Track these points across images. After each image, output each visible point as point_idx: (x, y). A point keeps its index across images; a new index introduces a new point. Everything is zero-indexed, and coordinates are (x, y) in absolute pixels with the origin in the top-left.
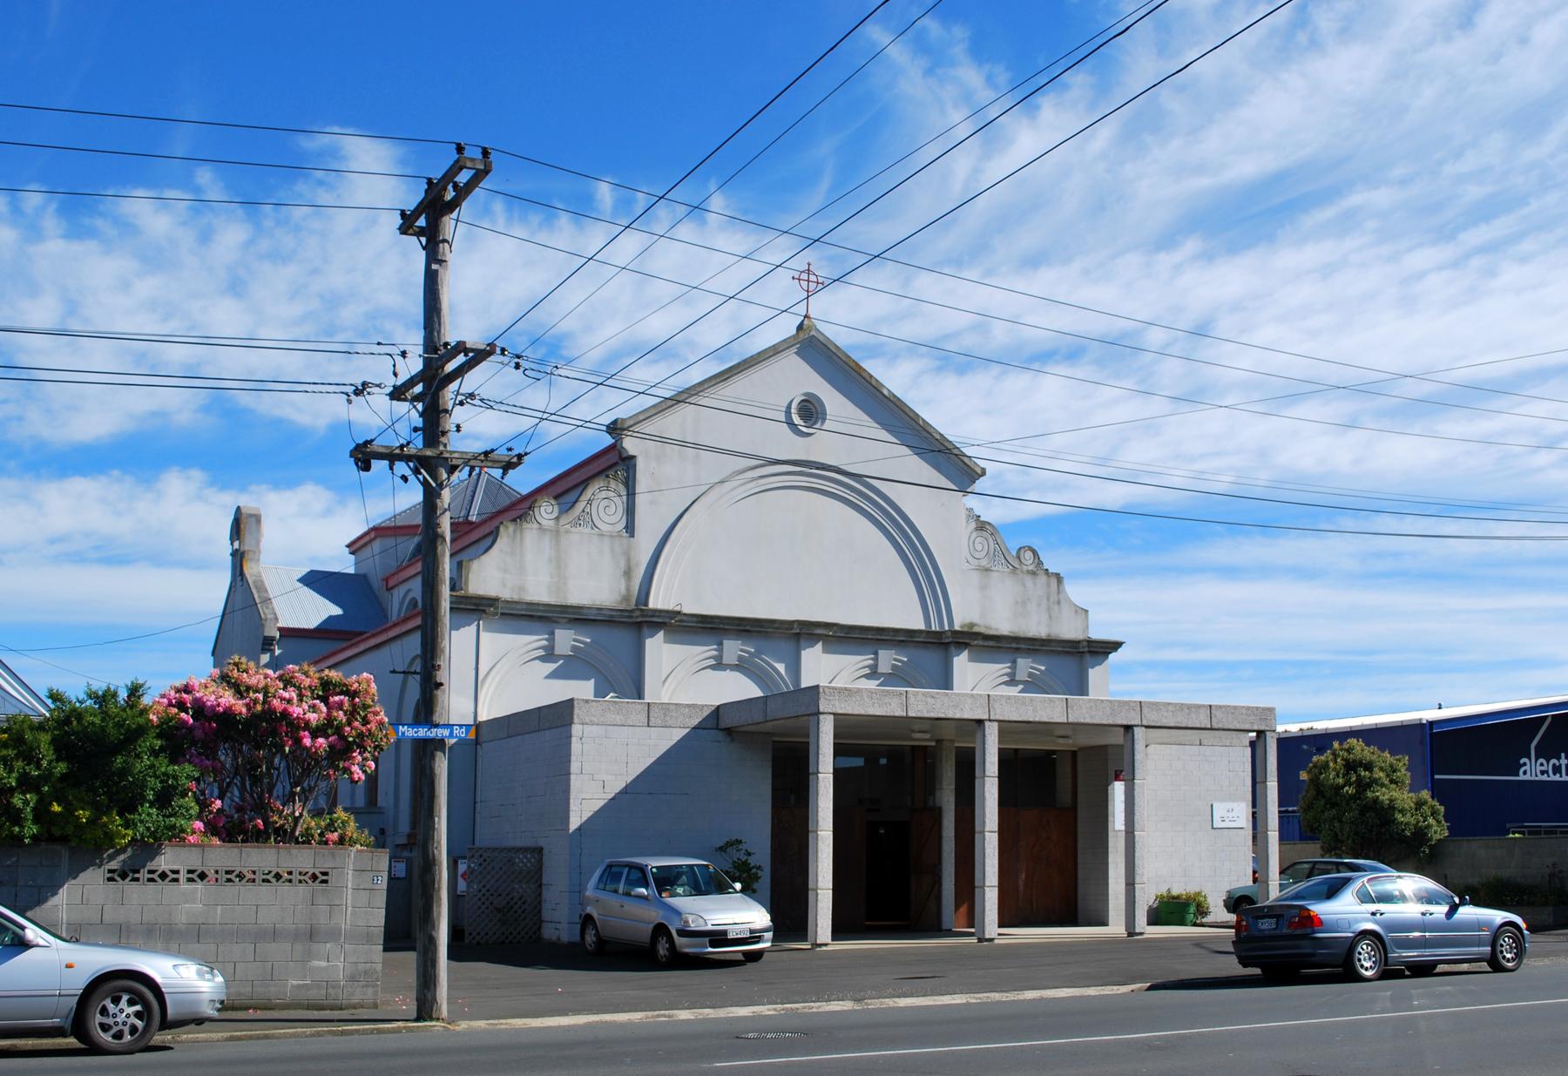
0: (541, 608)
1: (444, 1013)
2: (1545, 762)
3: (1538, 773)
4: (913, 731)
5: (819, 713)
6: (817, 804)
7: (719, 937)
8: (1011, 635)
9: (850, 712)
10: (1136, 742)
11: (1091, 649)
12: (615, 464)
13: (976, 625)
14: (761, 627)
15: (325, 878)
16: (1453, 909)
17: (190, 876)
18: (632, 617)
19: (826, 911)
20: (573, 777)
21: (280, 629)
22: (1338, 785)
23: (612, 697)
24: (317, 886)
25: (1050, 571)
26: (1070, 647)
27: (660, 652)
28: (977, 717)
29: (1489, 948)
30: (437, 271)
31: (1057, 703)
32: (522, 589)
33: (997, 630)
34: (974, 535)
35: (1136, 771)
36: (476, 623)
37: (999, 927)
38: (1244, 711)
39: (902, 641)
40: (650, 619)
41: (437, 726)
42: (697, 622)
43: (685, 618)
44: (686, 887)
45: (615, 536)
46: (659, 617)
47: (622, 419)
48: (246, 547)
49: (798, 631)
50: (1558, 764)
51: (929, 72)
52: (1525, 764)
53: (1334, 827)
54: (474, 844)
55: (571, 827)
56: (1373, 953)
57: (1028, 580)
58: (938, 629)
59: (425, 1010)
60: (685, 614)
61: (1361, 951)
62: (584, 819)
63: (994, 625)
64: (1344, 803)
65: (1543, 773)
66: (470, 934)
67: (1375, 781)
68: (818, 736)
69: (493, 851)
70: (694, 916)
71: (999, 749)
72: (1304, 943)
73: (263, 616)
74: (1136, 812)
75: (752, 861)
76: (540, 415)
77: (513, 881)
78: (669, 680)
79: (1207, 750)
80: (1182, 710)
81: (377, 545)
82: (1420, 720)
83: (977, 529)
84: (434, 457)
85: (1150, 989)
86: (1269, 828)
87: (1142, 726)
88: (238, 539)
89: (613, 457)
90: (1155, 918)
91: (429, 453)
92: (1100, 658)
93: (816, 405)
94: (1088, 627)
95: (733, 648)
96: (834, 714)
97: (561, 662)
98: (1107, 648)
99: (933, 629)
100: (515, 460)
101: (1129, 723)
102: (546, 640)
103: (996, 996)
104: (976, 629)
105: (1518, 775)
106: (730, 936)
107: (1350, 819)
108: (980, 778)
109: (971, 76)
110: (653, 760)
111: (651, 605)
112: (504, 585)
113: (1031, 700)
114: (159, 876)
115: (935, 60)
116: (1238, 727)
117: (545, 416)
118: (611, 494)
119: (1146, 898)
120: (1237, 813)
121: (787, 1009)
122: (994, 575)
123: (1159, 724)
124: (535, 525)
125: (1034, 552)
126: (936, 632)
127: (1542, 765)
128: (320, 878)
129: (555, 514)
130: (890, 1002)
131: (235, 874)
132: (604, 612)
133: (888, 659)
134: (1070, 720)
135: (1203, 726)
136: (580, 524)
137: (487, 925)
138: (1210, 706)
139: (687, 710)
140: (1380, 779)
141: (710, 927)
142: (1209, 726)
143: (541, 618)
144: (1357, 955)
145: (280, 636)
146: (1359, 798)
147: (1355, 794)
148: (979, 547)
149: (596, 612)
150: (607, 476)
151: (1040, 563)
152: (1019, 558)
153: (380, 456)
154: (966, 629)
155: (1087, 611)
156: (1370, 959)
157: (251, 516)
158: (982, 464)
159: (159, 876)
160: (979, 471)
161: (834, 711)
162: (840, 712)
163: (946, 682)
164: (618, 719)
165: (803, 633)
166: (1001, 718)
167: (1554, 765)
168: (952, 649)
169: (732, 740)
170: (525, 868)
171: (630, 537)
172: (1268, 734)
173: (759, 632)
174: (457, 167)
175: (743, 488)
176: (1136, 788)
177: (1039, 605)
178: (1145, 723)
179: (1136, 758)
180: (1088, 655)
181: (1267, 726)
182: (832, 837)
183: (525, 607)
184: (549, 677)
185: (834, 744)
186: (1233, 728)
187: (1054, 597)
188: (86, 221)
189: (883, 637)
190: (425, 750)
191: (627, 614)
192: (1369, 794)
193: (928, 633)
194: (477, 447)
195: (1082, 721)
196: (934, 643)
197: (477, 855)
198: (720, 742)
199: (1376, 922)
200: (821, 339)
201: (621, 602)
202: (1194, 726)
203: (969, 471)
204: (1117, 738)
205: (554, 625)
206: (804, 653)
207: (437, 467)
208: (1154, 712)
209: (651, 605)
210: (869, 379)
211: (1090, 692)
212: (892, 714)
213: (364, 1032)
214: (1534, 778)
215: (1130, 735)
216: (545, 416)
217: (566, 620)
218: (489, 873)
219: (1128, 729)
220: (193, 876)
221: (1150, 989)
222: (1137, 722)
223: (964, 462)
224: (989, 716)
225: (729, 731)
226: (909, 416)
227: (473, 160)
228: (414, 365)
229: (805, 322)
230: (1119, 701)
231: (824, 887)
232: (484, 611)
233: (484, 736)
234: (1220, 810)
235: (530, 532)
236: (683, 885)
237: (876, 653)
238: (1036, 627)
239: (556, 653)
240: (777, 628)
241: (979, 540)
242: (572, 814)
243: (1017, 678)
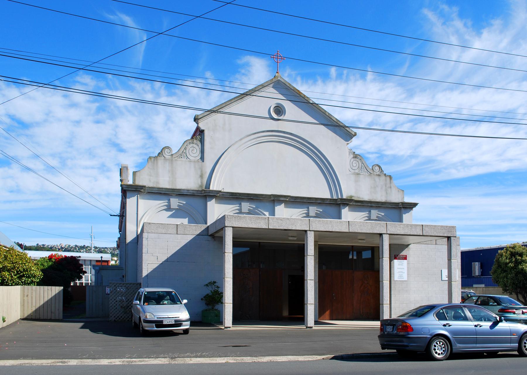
0: (164, 190)
4: (289, 236)
7: (159, 323)
8: (369, 200)
9: (240, 226)
11: (404, 206)
13: (353, 196)
14: (258, 197)
16: (496, 323)
18: (202, 193)
20: (143, 254)
22: (506, 262)
25: (387, 174)
26: (394, 206)
29: (517, 345)
32: (158, 183)
33: (362, 198)
35: (384, 254)
36: (137, 196)
38: (440, 228)
39: (320, 203)
42: (231, 195)
43: (225, 194)
44: (169, 301)
45: (196, 162)
46: (212, 193)
47: (197, 115)
49: (273, 199)
51: (444, 24)
53: (504, 280)
55: (143, 275)
56: (443, 346)
57: (377, 178)
58: (336, 198)
61: (436, 345)
62: (149, 272)
64: (509, 270)
66: (111, 317)
69: (130, 284)
70: (150, 314)
72: (404, 340)
74: (384, 272)
77: (118, 296)
80: (408, 227)
83: (353, 158)
85: (333, 358)
86: (452, 281)
87: (387, 234)
92: (408, 210)
93: (283, 109)
96: (233, 227)
97: (174, 211)
98: (411, 206)
99: (334, 198)
102: (167, 202)
104: (353, 198)
106: (165, 323)
107: (511, 277)
108: (381, 258)
109: (458, 24)
110: (180, 248)
111: (211, 188)
112: (150, 181)
113: (331, 222)
115: (446, 19)
116: (437, 235)
118: (194, 145)
122: (361, 176)
124: (163, 158)
125: (379, 167)
132: (190, 191)
134: (350, 231)
135: (418, 234)
136: (182, 157)
137: (118, 313)
138: (422, 225)
139: (194, 227)
140: (526, 260)
141: (156, 319)
142: (422, 235)
144: (433, 346)
146: (516, 268)
147: (514, 266)
148: (355, 165)
149: (187, 191)
151: (382, 171)
152: (373, 169)
154: (349, 198)
156: (441, 349)
157: (125, 167)
158: (355, 130)
160: (354, 134)
161: (232, 226)
166: (316, 230)
168: (342, 206)
169: (215, 240)
170: (123, 291)
171: (203, 162)
172: (452, 238)
173: (257, 199)
175: (249, 142)
179: (384, 248)
180: (403, 208)
181: (451, 234)
182: (232, 281)
183: (157, 189)
184: (169, 217)
186: (434, 235)
187: (388, 185)
188: (173, 91)
189: (311, 201)
191: (200, 192)
192: (520, 267)
195: (356, 231)
196: (334, 204)
199: (446, 330)
200: (283, 81)
202: (413, 234)
203: (350, 134)
205: (171, 197)
206: (276, 208)
208: (394, 228)
209: (211, 188)
211: (342, 218)
215: (381, 238)
217: (175, 195)
218: (127, 294)
221: (333, 358)
222: (385, 232)
223: (347, 130)
224: (310, 229)
226: (322, 112)
231: (228, 302)
236: (167, 300)
237: (308, 208)
238: (380, 197)
240: (264, 198)
241: (354, 162)
242: (143, 269)
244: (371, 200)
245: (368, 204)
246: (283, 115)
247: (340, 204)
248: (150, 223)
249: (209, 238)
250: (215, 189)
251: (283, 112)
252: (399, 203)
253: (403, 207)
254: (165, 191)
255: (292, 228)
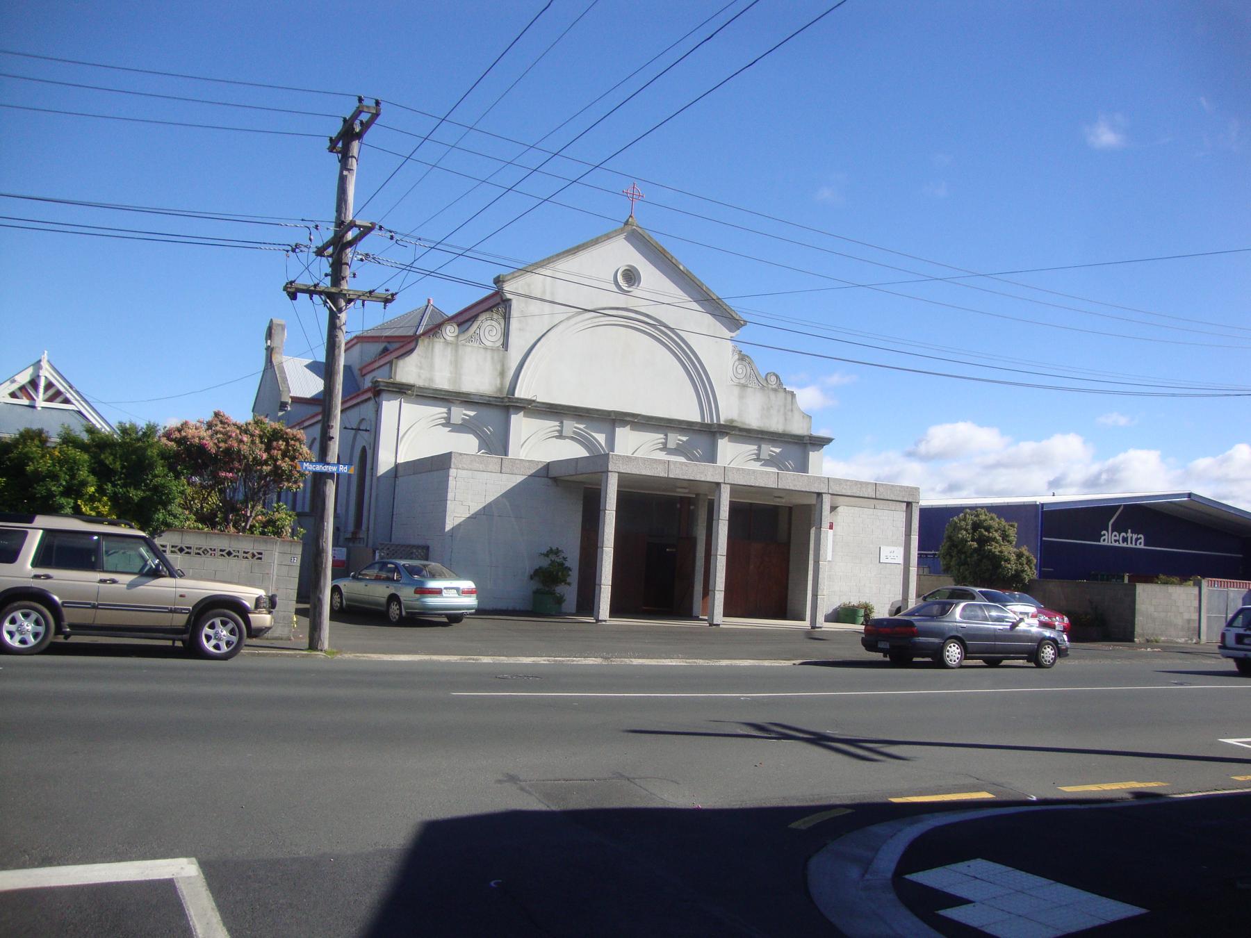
1: (326, 645)
2: (1118, 535)
3: (1113, 541)
5: (608, 471)
6: (604, 530)
10: (823, 504)
12: (499, 304)
13: (735, 421)
15: (260, 556)
17: (173, 549)
19: (606, 599)
20: (449, 502)
21: (292, 397)
23: (483, 453)
24: (255, 561)
27: (520, 424)
28: (717, 481)
30: (346, 176)
31: (772, 474)
32: (431, 380)
33: (749, 425)
34: (737, 363)
35: (823, 523)
36: (399, 400)
37: (724, 616)
38: (898, 489)
40: (515, 404)
41: (328, 464)
42: (548, 408)
43: (538, 405)
48: (274, 345)
50: (1126, 536)
52: (1104, 535)
54: (391, 541)
57: (772, 395)
59: (313, 645)
60: (538, 402)
63: (747, 421)
65: (1116, 541)
67: (994, 539)
68: (607, 485)
71: (730, 501)
73: (281, 389)
75: (567, 564)
76: (412, 269)
78: (526, 444)
79: (879, 512)
81: (358, 347)
82: (1036, 502)
83: (739, 359)
84: (336, 293)
86: (911, 565)
88: (270, 339)
89: (497, 299)
90: (829, 618)
91: (334, 290)
94: (811, 427)
95: (571, 426)
98: (823, 442)
100: (390, 297)
101: (820, 491)
103: (701, 662)
104: (735, 424)
105: (1100, 541)
111: (517, 395)
112: (420, 376)
114: (231, 554)
117: (409, 268)
118: (494, 323)
119: (825, 607)
120: (896, 554)
121: (556, 661)
122: (749, 390)
123: (840, 493)
124: (442, 340)
125: (777, 377)
126: (708, 424)
127: (1115, 536)
128: (258, 556)
129: (456, 334)
130: (627, 661)
131: (202, 550)
133: (676, 439)
134: (779, 487)
135: (870, 496)
138: (876, 484)
143: (442, 399)
145: (292, 401)
148: (740, 371)
150: (492, 311)
151: (781, 384)
153: (303, 291)
155: (810, 417)
159: (231, 554)
162: (623, 471)
163: (712, 458)
164: (481, 467)
165: (612, 420)
166: (733, 483)
167: (1123, 537)
168: (718, 435)
169: (557, 485)
172: (913, 504)
174: (359, 112)
175: (581, 324)
176: (822, 532)
177: (779, 411)
178: (830, 492)
185: (618, 491)
187: (789, 407)
190: (319, 479)
193: (702, 424)
194: (321, 289)
195: (788, 488)
197: (386, 548)
198: (548, 486)
201: (496, 392)
202: (864, 496)
204: (813, 501)
205: (452, 404)
207: (338, 299)
209: (517, 395)
210: (670, 258)
212: (658, 475)
213: (273, 655)
214: (1110, 544)
215: (820, 500)
216: (409, 268)
217: (459, 402)
219: (819, 495)
220: (176, 550)
225: (555, 479)
227: (368, 107)
228: (328, 233)
229: (630, 220)
230: (814, 477)
232: (405, 393)
233: (401, 472)
234: (885, 551)
235: (438, 345)
239: (451, 422)
241: (740, 366)
243: (761, 457)
244: (763, 429)
245: (758, 434)
246: (636, 285)
247: (715, 432)
248: (461, 454)
249: (550, 481)
250: (522, 397)
251: (635, 278)
252: (804, 437)
253: (810, 443)
254: (444, 395)
255: (701, 477)
